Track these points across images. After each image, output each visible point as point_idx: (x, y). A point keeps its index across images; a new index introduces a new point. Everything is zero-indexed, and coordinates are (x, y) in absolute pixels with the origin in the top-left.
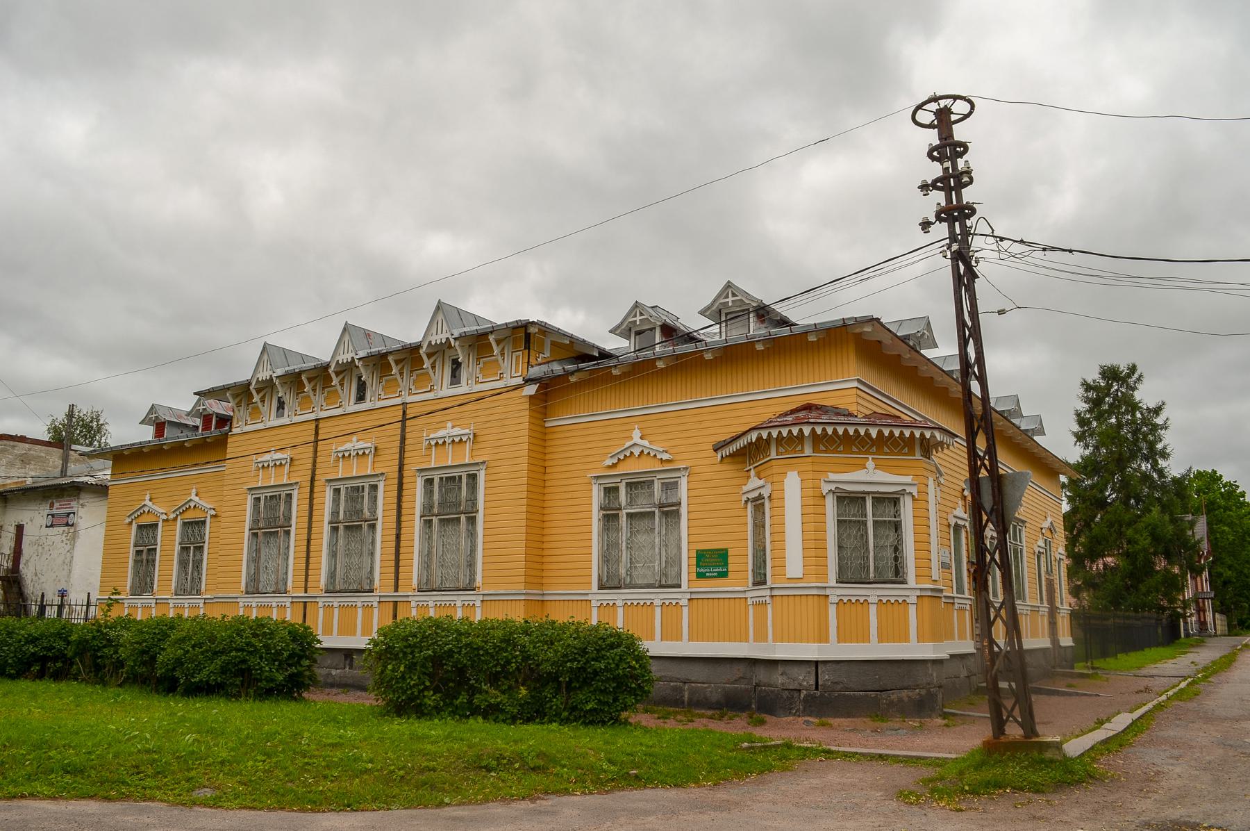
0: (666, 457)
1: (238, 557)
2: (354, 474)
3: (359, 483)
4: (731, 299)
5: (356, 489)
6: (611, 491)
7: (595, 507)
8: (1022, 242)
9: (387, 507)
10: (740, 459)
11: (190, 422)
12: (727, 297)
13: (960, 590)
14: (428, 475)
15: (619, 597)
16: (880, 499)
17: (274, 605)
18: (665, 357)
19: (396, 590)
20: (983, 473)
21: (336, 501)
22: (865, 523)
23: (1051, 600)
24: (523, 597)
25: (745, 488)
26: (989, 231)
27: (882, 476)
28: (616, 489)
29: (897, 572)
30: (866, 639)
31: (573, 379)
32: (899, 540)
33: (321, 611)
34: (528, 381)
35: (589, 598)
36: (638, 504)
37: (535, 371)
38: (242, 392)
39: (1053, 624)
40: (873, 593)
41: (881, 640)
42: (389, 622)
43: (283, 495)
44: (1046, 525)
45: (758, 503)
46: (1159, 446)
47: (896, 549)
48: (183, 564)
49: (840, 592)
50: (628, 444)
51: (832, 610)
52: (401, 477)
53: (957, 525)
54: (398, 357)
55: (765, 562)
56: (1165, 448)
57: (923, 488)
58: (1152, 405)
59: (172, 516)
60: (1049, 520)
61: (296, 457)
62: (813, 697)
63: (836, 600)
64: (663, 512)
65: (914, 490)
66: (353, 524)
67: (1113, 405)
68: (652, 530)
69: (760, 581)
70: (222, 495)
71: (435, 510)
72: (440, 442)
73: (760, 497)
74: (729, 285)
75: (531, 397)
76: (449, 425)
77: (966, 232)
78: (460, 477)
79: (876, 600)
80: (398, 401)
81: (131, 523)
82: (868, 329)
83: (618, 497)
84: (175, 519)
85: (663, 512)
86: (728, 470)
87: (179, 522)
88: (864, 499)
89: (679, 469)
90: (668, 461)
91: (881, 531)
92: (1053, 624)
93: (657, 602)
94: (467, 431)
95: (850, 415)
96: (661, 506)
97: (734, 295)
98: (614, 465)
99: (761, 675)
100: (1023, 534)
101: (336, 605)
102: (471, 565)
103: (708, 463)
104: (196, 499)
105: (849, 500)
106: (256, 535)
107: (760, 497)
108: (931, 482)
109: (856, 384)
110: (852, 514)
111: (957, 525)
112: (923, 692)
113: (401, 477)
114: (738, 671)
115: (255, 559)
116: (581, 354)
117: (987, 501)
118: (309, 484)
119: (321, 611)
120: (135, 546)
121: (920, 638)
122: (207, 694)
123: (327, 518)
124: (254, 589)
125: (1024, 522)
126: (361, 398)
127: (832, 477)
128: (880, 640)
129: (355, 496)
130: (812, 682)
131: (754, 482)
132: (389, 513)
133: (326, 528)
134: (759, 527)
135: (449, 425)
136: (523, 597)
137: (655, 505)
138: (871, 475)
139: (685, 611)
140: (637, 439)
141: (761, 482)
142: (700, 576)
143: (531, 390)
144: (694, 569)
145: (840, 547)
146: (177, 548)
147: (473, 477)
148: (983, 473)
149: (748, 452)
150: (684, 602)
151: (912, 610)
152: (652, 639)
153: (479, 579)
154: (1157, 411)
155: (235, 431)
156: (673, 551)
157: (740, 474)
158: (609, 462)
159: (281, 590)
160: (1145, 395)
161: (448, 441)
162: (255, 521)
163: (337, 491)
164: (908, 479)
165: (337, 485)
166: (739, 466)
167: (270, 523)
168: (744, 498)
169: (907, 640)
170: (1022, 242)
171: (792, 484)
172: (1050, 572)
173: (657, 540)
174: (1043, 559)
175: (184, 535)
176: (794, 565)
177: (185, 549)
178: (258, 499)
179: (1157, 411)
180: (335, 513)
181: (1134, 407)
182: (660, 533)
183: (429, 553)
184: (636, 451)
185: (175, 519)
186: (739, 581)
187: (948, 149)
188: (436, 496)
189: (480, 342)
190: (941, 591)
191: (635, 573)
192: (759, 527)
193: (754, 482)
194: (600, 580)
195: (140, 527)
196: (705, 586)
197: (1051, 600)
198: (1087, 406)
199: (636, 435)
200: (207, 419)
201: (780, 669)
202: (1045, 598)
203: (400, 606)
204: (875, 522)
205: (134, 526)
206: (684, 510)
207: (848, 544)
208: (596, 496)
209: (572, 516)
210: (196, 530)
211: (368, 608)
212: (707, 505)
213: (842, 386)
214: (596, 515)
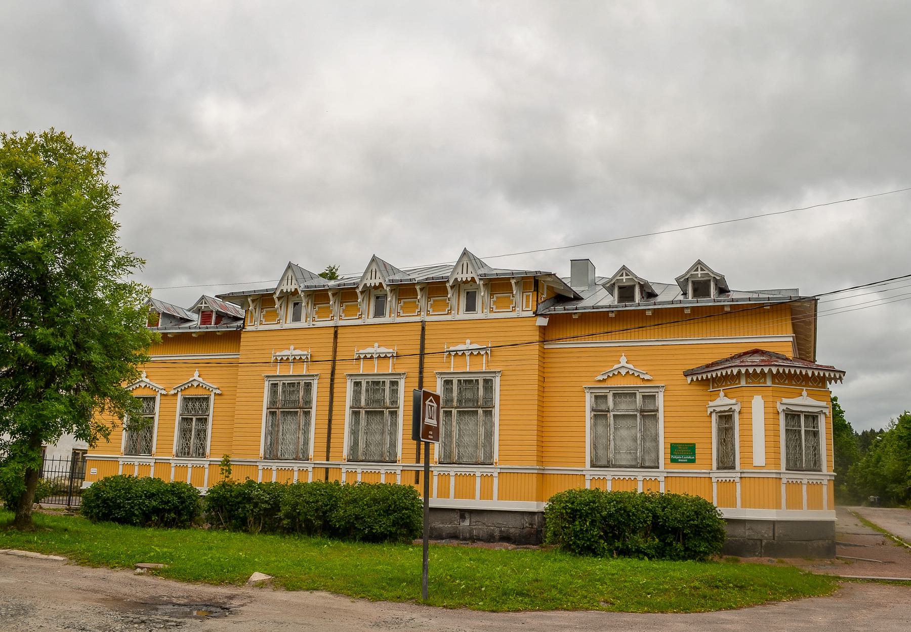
0: (647, 377)
3: (473, 377)
5: (378, 383)
6: (600, 398)
12: (697, 270)
14: (448, 377)
19: (328, 460)
27: (727, 401)
28: (605, 397)
29: (815, 464)
30: (473, 497)
33: (173, 469)
35: (584, 473)
38: (264, 300)
42: (220, 478)
43: (302, 383)
48: (185, 433)
50: (616, 366)
51: (783, 488)
59: (172, 392)
64: (643, 416)
68: (636, 427)
69: (726, 463)
71: (455, 404)
74: (624, 268)
80: (331, 323)
83: (607, 402)
84: (176, 394)
85: (643, 416)
86: (697, 390)
88: (799, 416)
89: (658, 387)
90: (648, 380)
94: (305, 353)
96: (642, 411)
97: (627, 275)
98: (604, 380)
103: (683, 386)
105: (792, 416)
112: (830, 542)
119: (173, 469)
122: (373, 542)
123: (349, 402)
124: (272, 454)
127: (785, 400)
130: (771, 535)
133: (348, 412)
136: (536, 471)
137: (637, 410)
140: (196, 377)
142: (673, 461)
146: (178, 418)
149: (711, 378)
153: (496, 457)
155: (248, 328)
157: (705, 393)
159: (302, 456)
162: (273, 403)
163: (357, 384)
166: (704, 388)
167: (289, 403)
168: (710, 410)
169: (821, 508)
171: (758, 404)
175: (185, 408)
176: (759, 457)
177: (186, 420)
184: (623, 372)
188: (455, 394)
189: (499, 284)
194: (592, 461)
195: (186, 400)
196: (677, 468)
199: (196, 374)
203: (330, 472)
214: (588, 414)
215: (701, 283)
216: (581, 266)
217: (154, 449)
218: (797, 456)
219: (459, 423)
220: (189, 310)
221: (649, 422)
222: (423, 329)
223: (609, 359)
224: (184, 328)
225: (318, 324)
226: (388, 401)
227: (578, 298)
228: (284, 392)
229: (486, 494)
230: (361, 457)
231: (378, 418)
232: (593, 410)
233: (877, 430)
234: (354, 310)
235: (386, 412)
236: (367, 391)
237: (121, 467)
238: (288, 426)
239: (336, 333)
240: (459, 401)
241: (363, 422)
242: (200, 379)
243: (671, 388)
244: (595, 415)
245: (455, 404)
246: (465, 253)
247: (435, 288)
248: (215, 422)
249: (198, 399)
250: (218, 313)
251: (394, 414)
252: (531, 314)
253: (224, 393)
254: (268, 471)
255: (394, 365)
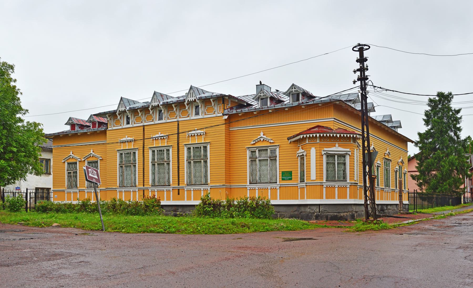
0: (272, 141)
1: (245, 167)
2: (127, 148)
4: (294, 90)
5: (161, 151)
7: (248, 158)
8: (380, 88)
9: (183, 161)
10: (296, 142)
11: (88, 124)
13: (396, 187)
14: (189, 146)
15: (256, 186)
16: (339, 156)
17: (131, 191)
18: (270, 107)
19: (179, 185)
20: (366, 152)
21: (153, 155)
22: (335, 163)
23: (400, 188)
24: (319, 184)
25: (298, 152)
26: (372, 84)
27: (340, 149)
29: (344, 178)
31: (240, 115)
32: (345, 168)
33: (186, 192)
34: (224, 115)
36: (263, 154)
37: (226, 112)
38: (113, 114)
39: (401, 196)
40: (337, 184)
41: (338, 198)
44: (387, 152)
45: (302, 157)
46: (458, 126)
47: (344, 171)
49: (327, 184)
51: (324, 189)
52: (178, 147)
53: (378, 166)
54: (176, 104)
55: (304, 175)
56: (460, 127)
57: (353, 152)
58: (457, 109)
59: (83, 160)
60: (401, 159)
61: (207, 132)
62: (318, 215)
63: (325, 186)
65: (350, 153)
66: (161, 162)
67: (441, 111)
69: (302, 180)
70: (108, 152)
71: (192, 158)
72: (193, 135)
73: (303, 155)
74: (293, 85)
75: (225, 119)
76: (127, 136)
77: (366, 84)
78: (201, 147)
79: (337, 186)
80: (141, 124)
81: (64, 162)
82: (338, 103)
84: (84, 161)
87: (66, 163)
88: (335, 156)
91: (340, 165)
92: (401, 196)
93: (269, 188)
94: (203, 131)
95: (331, 129)
98: (254, 144)
99: (302, 209)
100: (390, 164)
101: (156, 190)
102: (206, 176)
104: (73, 155)
105: (330, 156)
106: (122, 167)
107: (303, 155)
108: (355, 151)
109: (333, 120)
110: (331, 160)
111: (378, 166)
113: (178, 147)
114: (295, 208)
115: (122, 175)
116: (240, 103)
117: (367, 160)
118: (142, 148)
119: (186, 192)
120: (67, 170)
121: (350, 198)
125: (391, 160)
126: (128, 123)
127: (325, 149)
128: (280, 199)
129: (130, 154)
130: (318, 210)
131: (301, 151)
132: (147, 169)
133: (186, 163)
134: (302, 164)
135: (127, 136)
137: (268, 157)
138: (337, 148)
139: (278, 190)
141: (303, 151)
142: (283, 179)
143: (226, 117)
144: (281, 177)
145: (327, 171)
147: (205, 148)
148: (366, 152)
149: (298, 140)
150: (278, 188)
151: (348, 189)
152: (164, 200)
154: (458, 111)
155: (109, 129)
156: (274, 172)
158: (253, 143)
160: (454, 105)
161: (196, 135)
163: (154, 151)
164: (348, 150)
165: (154, 149)
167: (127, 160)
168: (297, 155)
169: (346, 198)
170: (380, 88)
171: (313, 151)
172: (400, 177)
173: (269, 168)
174: (398, 173)
178: (122, 154)
179: (458, 111)
180: (153, 159)
181: (450, 109)
182: (270, 166)
183: (190, 173)
184: (92, 155)
185: (84, 161)
186: (296, 180)
187: (362, 60)
188: (192, 154)
189: (206, 101)
190: (357, 184)
191: (261, 179)
192: (302, 164)
193: (301, 151)
194: (250, 181)
195: (68, 163)
197: (400, 188)
198: (430, 108)
200: (94, 123)
201: (309, 207)
202: (398, 186)
203: (145, 191)
204: (338, 163)
205: (66, 163)
206: (278, 158)
207: (329, 169)
208: (248, 153)
209: (285, 153)
210: (73, 166)
211: (134, 192)
212: (284, 158)
213: (330, 120)
214: (248, 160)
215: (296, 93)
216: (15, 81)
217: (78, 185)
218: (274, 172)
219: (194, 167)
220: (284, 94)
221: (273, 162)
222: (178, 124)
223: (256, 134)
224: (85, 130)
225: (135, 125)
226: (166, 159)
227: (284, 101)
228: (125, 157)
229: (69, 199)
230: (156, 185)
231: (162, 167)
232: (250, 158)
233: (367, 73)
234: (150, 118)
235: (165, 163)
236: (157, 154)
237: (150, 193)
238: (254, 163)
239: (144, 129)
240: (194, 156)
241: (156, 169)
242: (93, 153)
243: (282, 146)
244: (251, 160)
245: (192, 158)
246: (375, 111)
247: (180, 104)
248: (280, 165)
249: (94, 162)
250: (99, 122)
251: (168, 164)
252: (221, 114)
253: (276, 142)
254: (252, 190)
255: (134, 145)
